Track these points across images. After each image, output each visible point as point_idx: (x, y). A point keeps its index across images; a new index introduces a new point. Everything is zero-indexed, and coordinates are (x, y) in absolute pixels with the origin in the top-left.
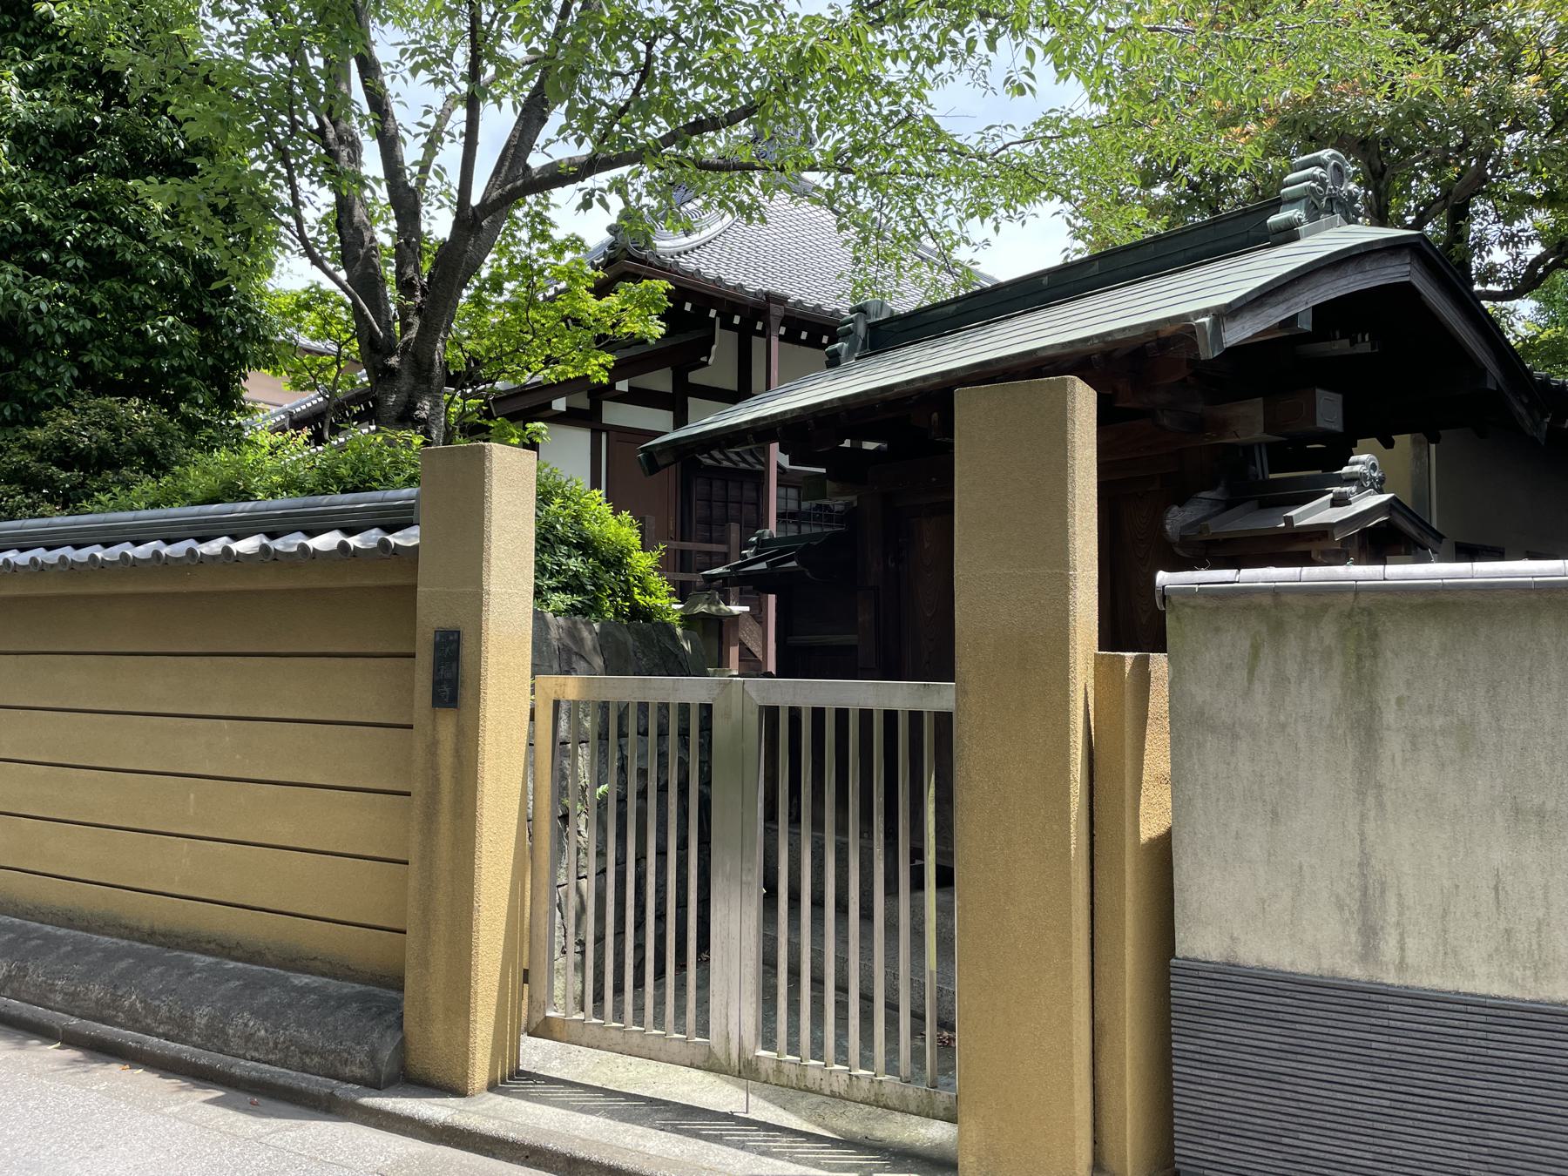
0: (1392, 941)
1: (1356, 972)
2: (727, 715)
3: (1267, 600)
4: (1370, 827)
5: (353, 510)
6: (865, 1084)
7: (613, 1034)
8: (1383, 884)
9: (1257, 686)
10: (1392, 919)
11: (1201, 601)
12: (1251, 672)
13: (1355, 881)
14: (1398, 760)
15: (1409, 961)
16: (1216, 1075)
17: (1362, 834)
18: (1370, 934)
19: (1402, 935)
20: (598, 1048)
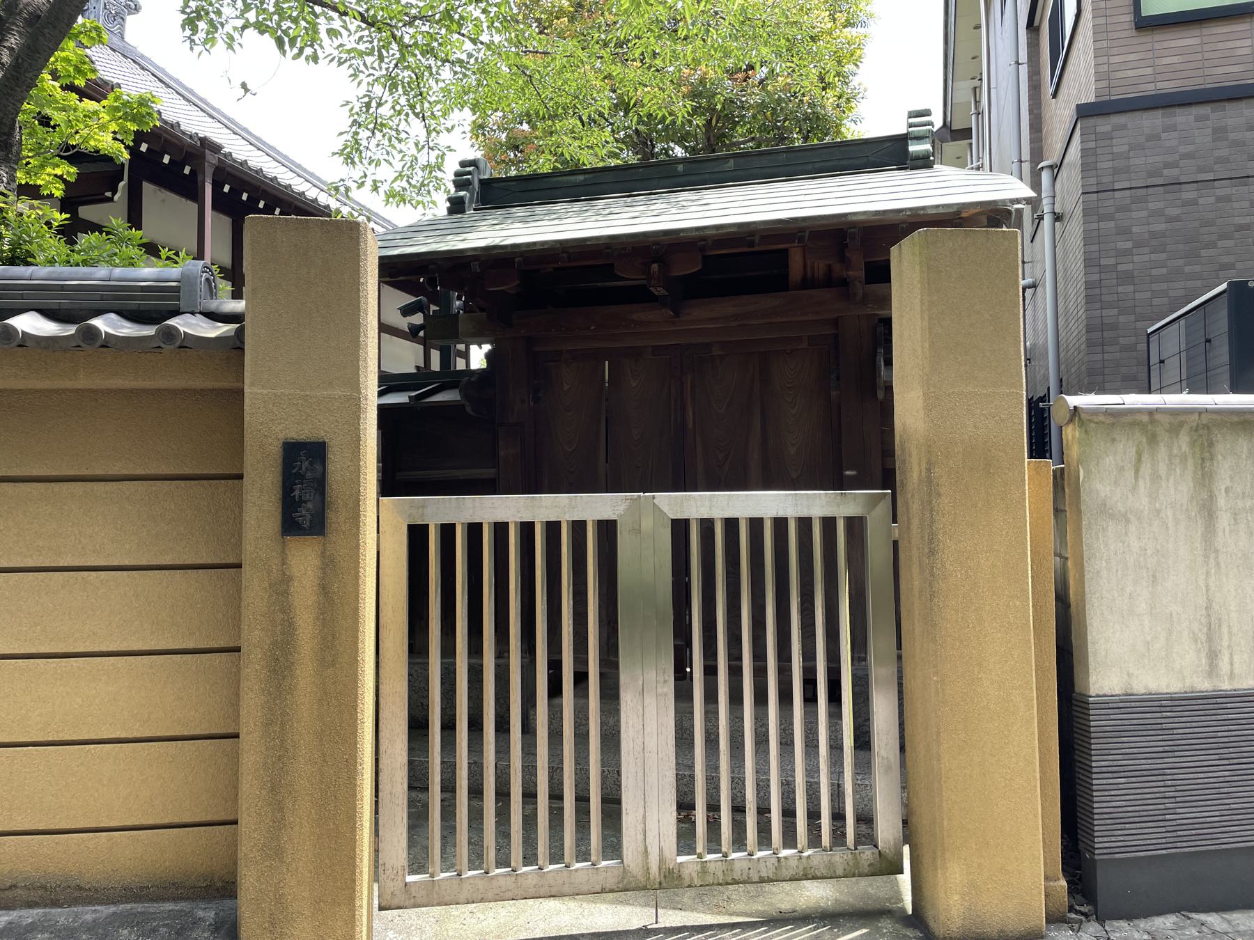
0: (1226, 659)
1: (1204, 685)
2: (637, 531)
3: (1145, 418)
4: (1212, 580)
5: (63, 288)
6: (794, 863)
7: (502, 881)
8: (1220, 620)
9: (1141, 482)
10: (1225, 643)
11: (1101, 418)
12: (1137, 471)
13: (1204, 620)
14: (1227, 531)
15: (1236, 671)
16: (1123, 780)
17: (1207, 586)
18: (1213, 655)
19: (1231, 654)
20: (482, 900)
